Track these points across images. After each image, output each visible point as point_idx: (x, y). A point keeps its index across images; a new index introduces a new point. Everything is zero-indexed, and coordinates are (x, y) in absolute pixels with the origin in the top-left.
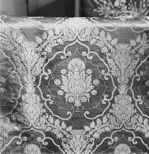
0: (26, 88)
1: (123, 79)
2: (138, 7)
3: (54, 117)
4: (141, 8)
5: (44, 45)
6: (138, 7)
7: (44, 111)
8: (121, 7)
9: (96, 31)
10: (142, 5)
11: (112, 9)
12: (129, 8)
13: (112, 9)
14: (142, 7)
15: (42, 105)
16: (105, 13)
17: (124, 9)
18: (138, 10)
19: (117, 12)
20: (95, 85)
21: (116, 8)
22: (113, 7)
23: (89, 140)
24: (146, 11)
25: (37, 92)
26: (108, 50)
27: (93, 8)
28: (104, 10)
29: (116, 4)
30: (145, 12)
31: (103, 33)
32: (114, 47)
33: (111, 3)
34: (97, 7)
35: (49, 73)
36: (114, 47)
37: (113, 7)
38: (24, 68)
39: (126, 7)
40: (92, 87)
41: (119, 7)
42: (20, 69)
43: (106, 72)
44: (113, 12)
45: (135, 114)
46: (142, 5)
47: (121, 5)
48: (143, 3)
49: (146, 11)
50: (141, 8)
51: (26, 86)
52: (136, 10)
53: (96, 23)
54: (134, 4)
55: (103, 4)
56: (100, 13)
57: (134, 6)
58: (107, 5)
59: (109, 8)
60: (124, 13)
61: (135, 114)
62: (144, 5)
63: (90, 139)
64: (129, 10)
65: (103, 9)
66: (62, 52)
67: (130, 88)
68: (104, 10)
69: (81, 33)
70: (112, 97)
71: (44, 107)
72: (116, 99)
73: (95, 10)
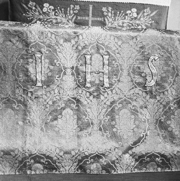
0: (66, 72)
1: (125, 66)
2: (66, 13)
3: (23, 89)
4: (68, 14)
5: (117, 46)
6: (66, 13)
7: (133, 86)
8: (49, 12)
9: (108, 37)
10: (70, 11)
11: (40, 14)
12: (56, 14)
13: (40, 14)
14: (70, 13)
15: (132, 83)
16: (34, 17)
17: (52, 15)
18: (66, 16)
19: (45, 17)
20: (51, 69)
21: (44, 13)
22: (41, 12)
23: (46, 106)
24: (73, 17)
25: (73, 74)
26: (116, 49)
27: (23, 13)
28: (32, 14)
29: (45, 10)
30: (72, 18)
31: (112, 38)
32: (120, 46)
33: (39, 9)
34: (27, 12)
35: (81, 63)
36: (120, 46)
37: (41, 12)
38: (65, 59)
39: (54, 13)
40: (162, 72)
41: (47, 13)
42: (121, 61)
43: (58, 61)
44: (41, 17)
45: (133, 88)
46: (70, 11)
47: (49, 11)
48: (70, 9)
49: (73, 17)
50: (68, 14)
51: (66, 70)
52: (64, 16)
53: (107, 31)
54: (61, 11)
55: (32, 9)
56: (29, 17)
57: (62, 13)
58: (35, 11)
59: (37, 13)
60: (52, 18)
61: (133, 88)
62: (72, 12)
63: (46, 105)
64: (57, 16)
65: (31, 14)
66: (88, 50)
67: (73, 71)
68: (32, 14)
69: (99, 38)
70: (61, 77)
71: (77, 84)
72: (64, 78)
73: (24, 14)
